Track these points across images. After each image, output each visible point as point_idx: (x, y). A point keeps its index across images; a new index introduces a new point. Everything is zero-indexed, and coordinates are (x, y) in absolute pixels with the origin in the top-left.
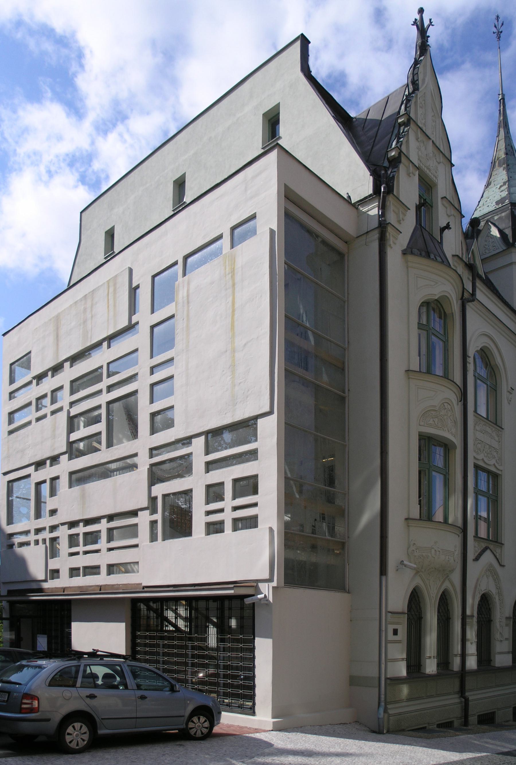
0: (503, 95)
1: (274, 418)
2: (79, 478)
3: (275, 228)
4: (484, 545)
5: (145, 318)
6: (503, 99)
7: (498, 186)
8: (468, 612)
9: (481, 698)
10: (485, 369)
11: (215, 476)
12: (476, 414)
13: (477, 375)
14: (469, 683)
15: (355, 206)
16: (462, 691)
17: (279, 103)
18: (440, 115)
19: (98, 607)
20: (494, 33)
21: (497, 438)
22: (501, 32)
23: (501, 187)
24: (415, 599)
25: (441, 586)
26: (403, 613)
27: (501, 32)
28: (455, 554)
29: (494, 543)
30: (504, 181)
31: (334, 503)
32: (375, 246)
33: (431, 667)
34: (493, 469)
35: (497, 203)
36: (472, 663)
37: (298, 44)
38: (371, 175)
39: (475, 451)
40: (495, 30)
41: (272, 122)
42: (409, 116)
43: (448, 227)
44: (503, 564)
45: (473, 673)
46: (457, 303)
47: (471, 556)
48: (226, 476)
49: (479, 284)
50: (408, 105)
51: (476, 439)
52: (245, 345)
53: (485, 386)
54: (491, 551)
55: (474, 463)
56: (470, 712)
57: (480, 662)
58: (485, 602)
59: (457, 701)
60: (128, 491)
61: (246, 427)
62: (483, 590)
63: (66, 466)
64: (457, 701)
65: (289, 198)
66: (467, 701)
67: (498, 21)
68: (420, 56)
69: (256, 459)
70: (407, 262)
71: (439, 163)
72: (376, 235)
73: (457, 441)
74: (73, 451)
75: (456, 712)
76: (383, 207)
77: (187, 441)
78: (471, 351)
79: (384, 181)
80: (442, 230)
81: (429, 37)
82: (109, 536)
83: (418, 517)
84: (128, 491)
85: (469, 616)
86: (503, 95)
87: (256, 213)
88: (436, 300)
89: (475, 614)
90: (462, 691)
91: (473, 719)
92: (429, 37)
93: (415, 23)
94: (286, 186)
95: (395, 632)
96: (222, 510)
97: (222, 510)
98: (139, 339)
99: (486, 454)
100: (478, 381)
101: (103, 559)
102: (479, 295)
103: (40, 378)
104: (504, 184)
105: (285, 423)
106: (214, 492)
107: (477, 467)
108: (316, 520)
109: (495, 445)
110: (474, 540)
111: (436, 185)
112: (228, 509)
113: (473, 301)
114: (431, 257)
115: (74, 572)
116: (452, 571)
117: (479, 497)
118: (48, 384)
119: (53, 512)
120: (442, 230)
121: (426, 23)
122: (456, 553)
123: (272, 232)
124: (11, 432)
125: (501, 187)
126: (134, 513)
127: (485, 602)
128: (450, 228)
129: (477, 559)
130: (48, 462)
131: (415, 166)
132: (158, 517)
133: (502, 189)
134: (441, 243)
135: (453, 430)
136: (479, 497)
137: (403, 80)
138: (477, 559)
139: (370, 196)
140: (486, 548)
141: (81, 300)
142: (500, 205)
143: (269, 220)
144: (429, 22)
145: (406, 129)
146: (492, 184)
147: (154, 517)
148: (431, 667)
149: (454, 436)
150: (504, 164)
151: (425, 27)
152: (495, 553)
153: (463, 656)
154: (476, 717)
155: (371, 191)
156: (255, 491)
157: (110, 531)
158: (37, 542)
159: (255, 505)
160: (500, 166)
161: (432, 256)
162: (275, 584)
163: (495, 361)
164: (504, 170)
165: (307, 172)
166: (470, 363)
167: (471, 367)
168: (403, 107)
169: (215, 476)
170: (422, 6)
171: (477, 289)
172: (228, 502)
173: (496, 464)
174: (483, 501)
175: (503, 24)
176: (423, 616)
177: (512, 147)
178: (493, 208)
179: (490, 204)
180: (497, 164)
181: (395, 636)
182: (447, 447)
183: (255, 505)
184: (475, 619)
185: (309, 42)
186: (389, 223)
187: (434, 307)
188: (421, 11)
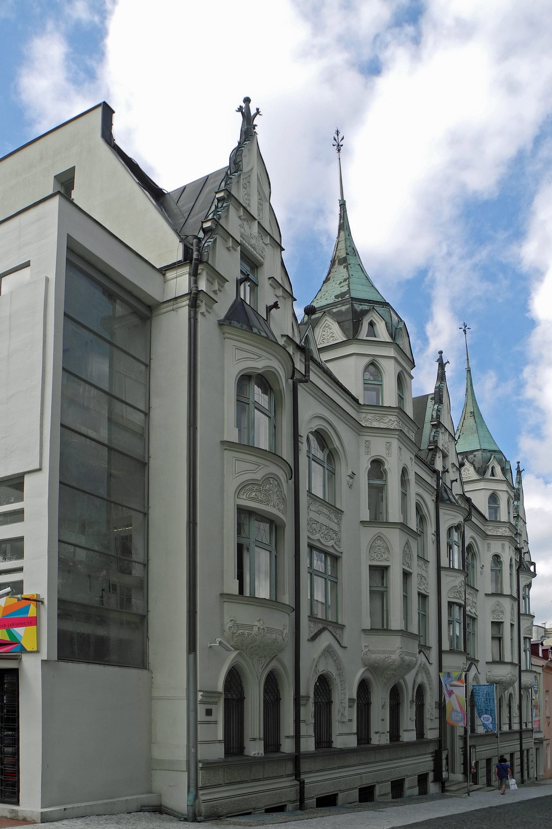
1: (45, 474)
3: (52, 277)
4: (321, 626)
7: (338, 282)
8: (303, 692)
9: (318, 781)
10: (321, 452)
12: (309, 494)
13: (311, 456)
14: (305, 766)
15: (163, 271)
16: (297, 774)
17: (75, 167)
18: (268, 199)
20: (334, 145)
21: (336, 521)
22: (342, 146)
23: (341, 283)
24: (234, 679)
25: (268, 665)
27: (342, 146)
28: (284, 634)
29: (334, 624)
30: (345, 277)
31: (130, 573)
33: (255, 749)
34: (331, 550)
35: (336, 297)
36: (308, 744)
37: (100, 110)
38: (180, 242)
39: (309, 531)
40: (335, 143)
41: (65, 183)
42: (230, 193)
43: (456, 480)
44: (344, 645)
45: (310, 756)
46: (287, 381)
47: (305, 634)
49: (312, 366)
50: (229, 182)
51: (311, 521)
53: (321, 468)
54: (329, 631)
55: (308, 542)
56: (306, 795)
57: (318, 744)
58: (324, 684)
62: (320, 671)
66: (302, 784)
67: (338, 135)
68: (245, 141)
69: (22, 520)
71: (266, 245)
73: (288, 520)
75: (292, 794)
76: (195, 274)
78: (303, 431)
80: (452, 482)
81: (256, 125)
82: (368, 720)
85: (303, 697)
87: (30, 261)
88: (259, 374)
89: (312, 695)
90: (297, 774)
91: (311, 802)
92: (256, 125)
93: (240, 109)
94: (69, 236)
95: (209, 712)
99: (322, 535)
100: (313, 462)
102: (313, 377)
105: (60, 482)
107: (311, 547)
108: (103, 590)
109: (336, 528)
110: (309, 620)
113: (306, 381)
114: (254, 331)
116: (281, 650)
117: (315, 577)
120: (452, 482)
121: (253, 112)
122: (286, 631)
125: (341, 283)
127: (324, 684)
128: (279, 308)
129: (313, 639)
131: (236, 241)
133: (342, 285)
134: (267, 321)
135: (282, 507)
136: (315, 577)
137: (226, 163)
138: (313, 639)
139: (179, 262)
140: (324, 629)
142: (340, 299)
144: (256, 111)
145: (224, 205)
148: (255, 749)
149: (282, 513)
151: (252, 115)
152: (335, 634)
153: (297, 737)
154: (315, 800)
155: (180, 257)
156: (20, 554)
159: (20, 569)
161: (255, 330)
162: (44, 656)
163: (333, 445)
164: (344, 268)
166: (302, 443)
167: (304, 447)
168: (223, 183)
170: (248, 96)
171: (310, 371)
173: (335, 546)
174: (319, 583)
175: (343, 139)
176: (245, 696)
177: (353, 248)
178: (332, 301)
179: (328, 298)
180: (337, 262)
181: (209, 717)
182: (275, 526)
183: (20, 569)
184: (312, 700)
185: (114, 112)
186: (202, 290)
188: (247, 100)
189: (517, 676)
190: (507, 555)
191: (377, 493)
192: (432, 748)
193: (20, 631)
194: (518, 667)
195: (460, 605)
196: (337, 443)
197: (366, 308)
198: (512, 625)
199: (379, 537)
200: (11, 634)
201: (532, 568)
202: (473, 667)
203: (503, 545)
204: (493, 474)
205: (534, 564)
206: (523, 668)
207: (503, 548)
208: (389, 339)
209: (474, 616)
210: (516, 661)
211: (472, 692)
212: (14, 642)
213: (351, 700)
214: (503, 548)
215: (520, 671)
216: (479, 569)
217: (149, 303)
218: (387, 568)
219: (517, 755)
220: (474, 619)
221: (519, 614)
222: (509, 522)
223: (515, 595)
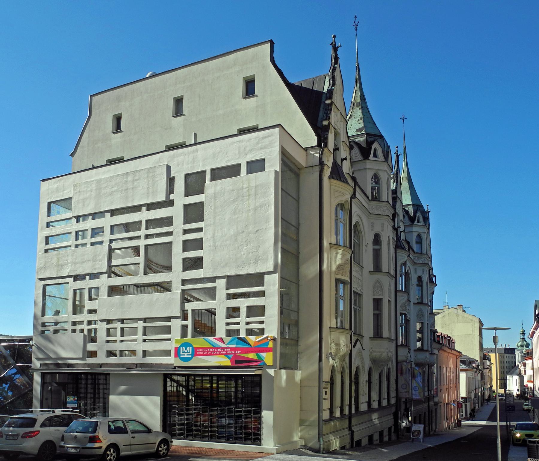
0: (358, 64)
1: (276, 276)
2: (113, 291)
3: (278, 169)
5: (180, 199)
6: (358, 65)
7: (357, 119)
11: (234, 303)
15: (306, 150)
19: (140, 377)
26: (328, 382)
32: (317, 174)
43: (346, 159)
48: (243, 304)
52: (257, 231)
59: (348, 433)
60: (167, 304)
61: (258, 279)
63: (104, 282)
64: (348, 433)
65: (284, 154)
66: (353, 432)
70: (330, 182)
72: (317, 169)
74: (111, 272)
77: (213, 279)
79: (322, 140)
80: (343, 160)
83: (335, 327)
84: (167, 304)
86: (358, 64)
96: (238, 323)
97: (238, 323)
98: (176, 211)
101: (140, 347)
102: (358, 195)
103: (78, 218)
104: (361, 119)
106: (233, 312)
109: (360, 278)
111: (340, 134)
112: (243, 324)
115: (111, 354)
118: (90, 224)
119: (91, 312)
120: (343, 160)
123: (276, 171)
124: (46, 251)
125: (358, 120)
126: (169, 319)
130: (87, 277)
132: (189, 322)
133: (360, 122)
139: (315, 146)
141: (123, 175)
143: (274, 165)
146: (353, 117)
147: (185, 323)
150: (359, 106)
157: (145, 328)
158: (74, 331)
160: (357, 106)
165: (287, 134)
169: (234, 303)
172: (243, 318)
187: (341, 206)
189: (394, 353)
190: (425, 278)
191: (377, 255)
192: (393, 409)
193: (263, 355)
194: (394, 342)
195: (344, 282)
196: (362, 228)
197: (373, 139)
198: (389, 301)
199: (378, 281)
200: (258, 356)
201: (434, 279)
202: (358, 342)
203: (423, 270)
204: (375, 156)
205: (435, 276)
206: (399, 343)
207: (423, 271)
208: (383, 160)
209: (359, 292)
210: (393, 337)
211: (357, 368)
212: (260, 360)
213: (366, 381)
214: (423, 271)
215: (397, 346)
216: (364, 247)
217: (299, 167)
218: (381, 299)
219: (427, 413)
220: (360, 295)
221: (396, 291)
222: (387, 202)
223: (393, 273)
